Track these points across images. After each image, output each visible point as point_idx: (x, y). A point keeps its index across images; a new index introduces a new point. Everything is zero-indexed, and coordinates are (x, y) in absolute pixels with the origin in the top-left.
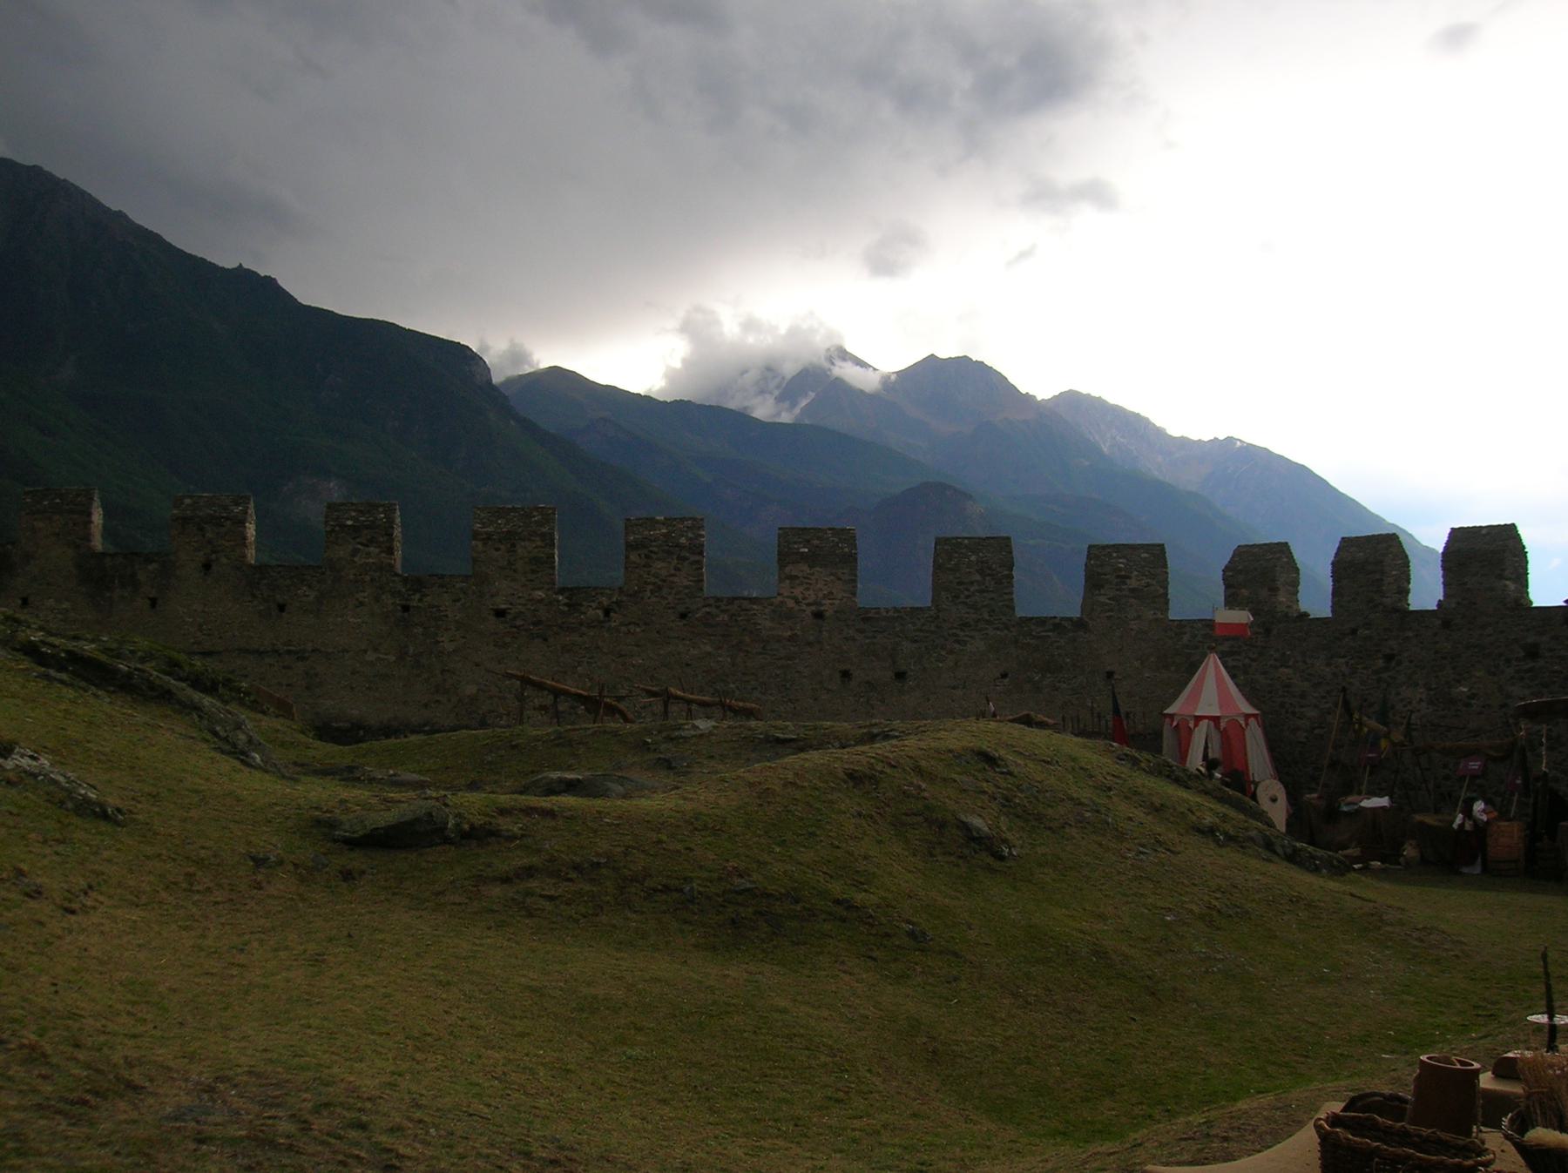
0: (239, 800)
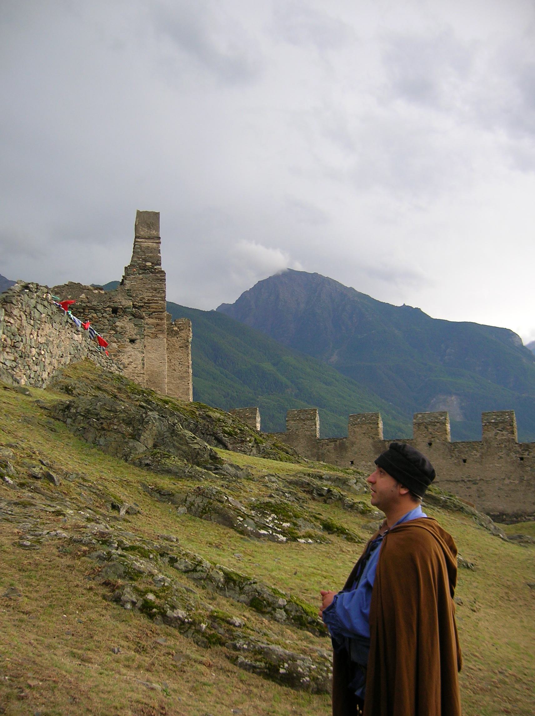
0: (513, 558)
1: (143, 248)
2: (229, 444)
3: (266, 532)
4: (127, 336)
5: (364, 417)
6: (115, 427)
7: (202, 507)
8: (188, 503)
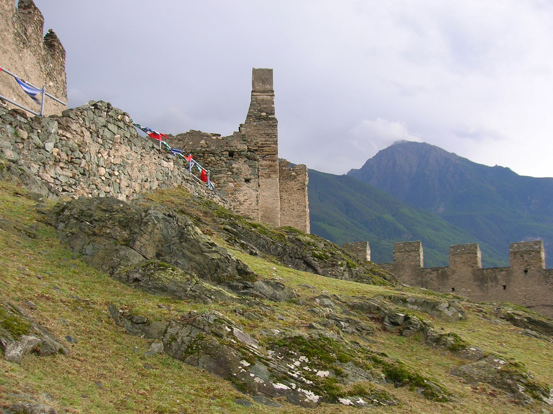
1: (258, 101)
2: (319, 268)
3: (285, 387)
4: (242, 176)
5: (464, 247)
6: (108, 231)
7: (187, 343)
8: (168, 336)
